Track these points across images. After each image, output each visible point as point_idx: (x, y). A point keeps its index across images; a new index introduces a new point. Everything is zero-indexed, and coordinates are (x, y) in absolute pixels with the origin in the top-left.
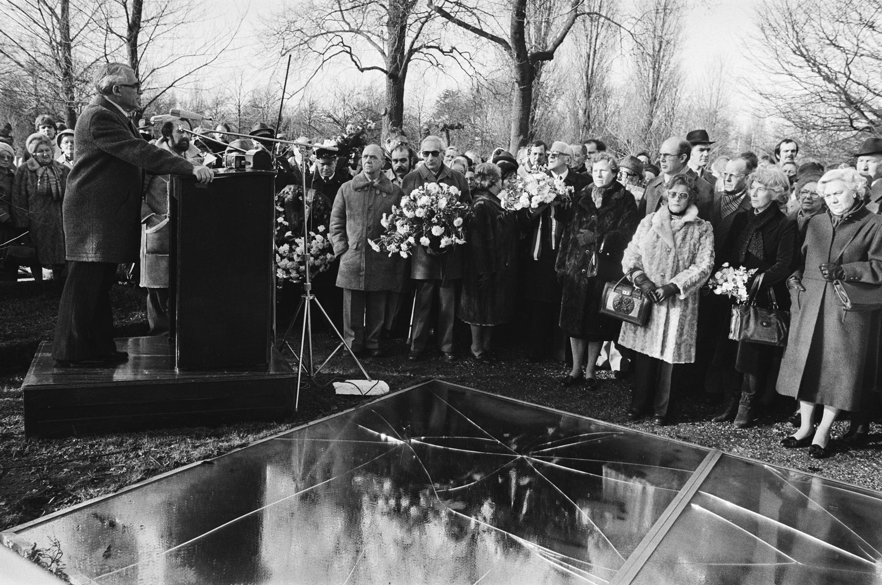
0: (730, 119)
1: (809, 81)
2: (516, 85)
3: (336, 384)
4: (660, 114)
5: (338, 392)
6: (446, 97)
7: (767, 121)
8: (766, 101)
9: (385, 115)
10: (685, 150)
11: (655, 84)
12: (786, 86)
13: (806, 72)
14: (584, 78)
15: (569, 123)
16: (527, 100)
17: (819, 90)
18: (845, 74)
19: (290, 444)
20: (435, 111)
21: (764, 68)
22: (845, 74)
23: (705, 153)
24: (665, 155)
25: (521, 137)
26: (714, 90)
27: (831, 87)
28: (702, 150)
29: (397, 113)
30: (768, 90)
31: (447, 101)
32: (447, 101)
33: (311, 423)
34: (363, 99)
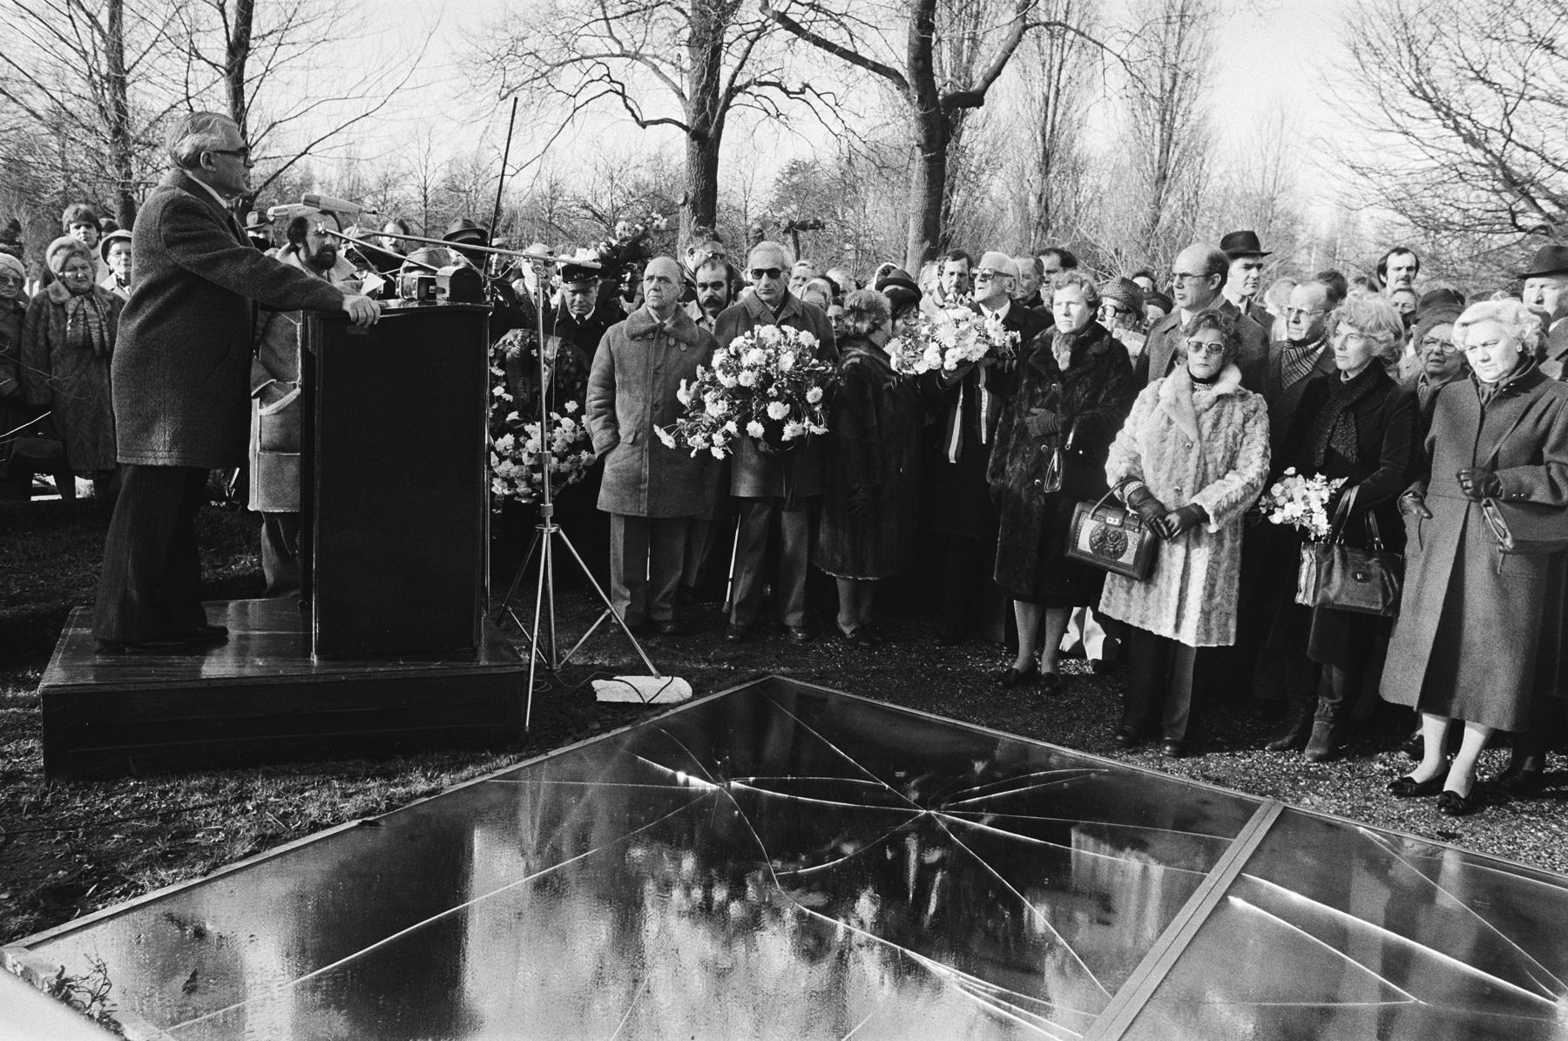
0: (1297, 212)
1: (1438, 143)
2: (918, 151)
3: (596, 684)
4: (1173, 202)
5: (601, 697)
6: (792, 172)
7: (1364, 215)
8: (1362, 180)
9: (684, 204)
10: (1217, 268)
11: (1165, 150)
12: (1398, 154)
13: (1432, 127)
14: (1039, 138)
15: (1011, 220)
16: (938, 179)
17: (1457, 159)
18: (1502, 131)
19: (516, 790)
20: (774, 198)
21: (1358, 121)
22: (1502, 131)
23: (1254, 272)
24: (1183, 276)
25: (927, 244)
26: (1270, 160)
27: (1478, 155)
28: (1248, 267)
29: (705, 201)
30: (1366, 159)
31: (795, 179)
32: (795, 179)
33: (553, 753)
34: (646, 176)
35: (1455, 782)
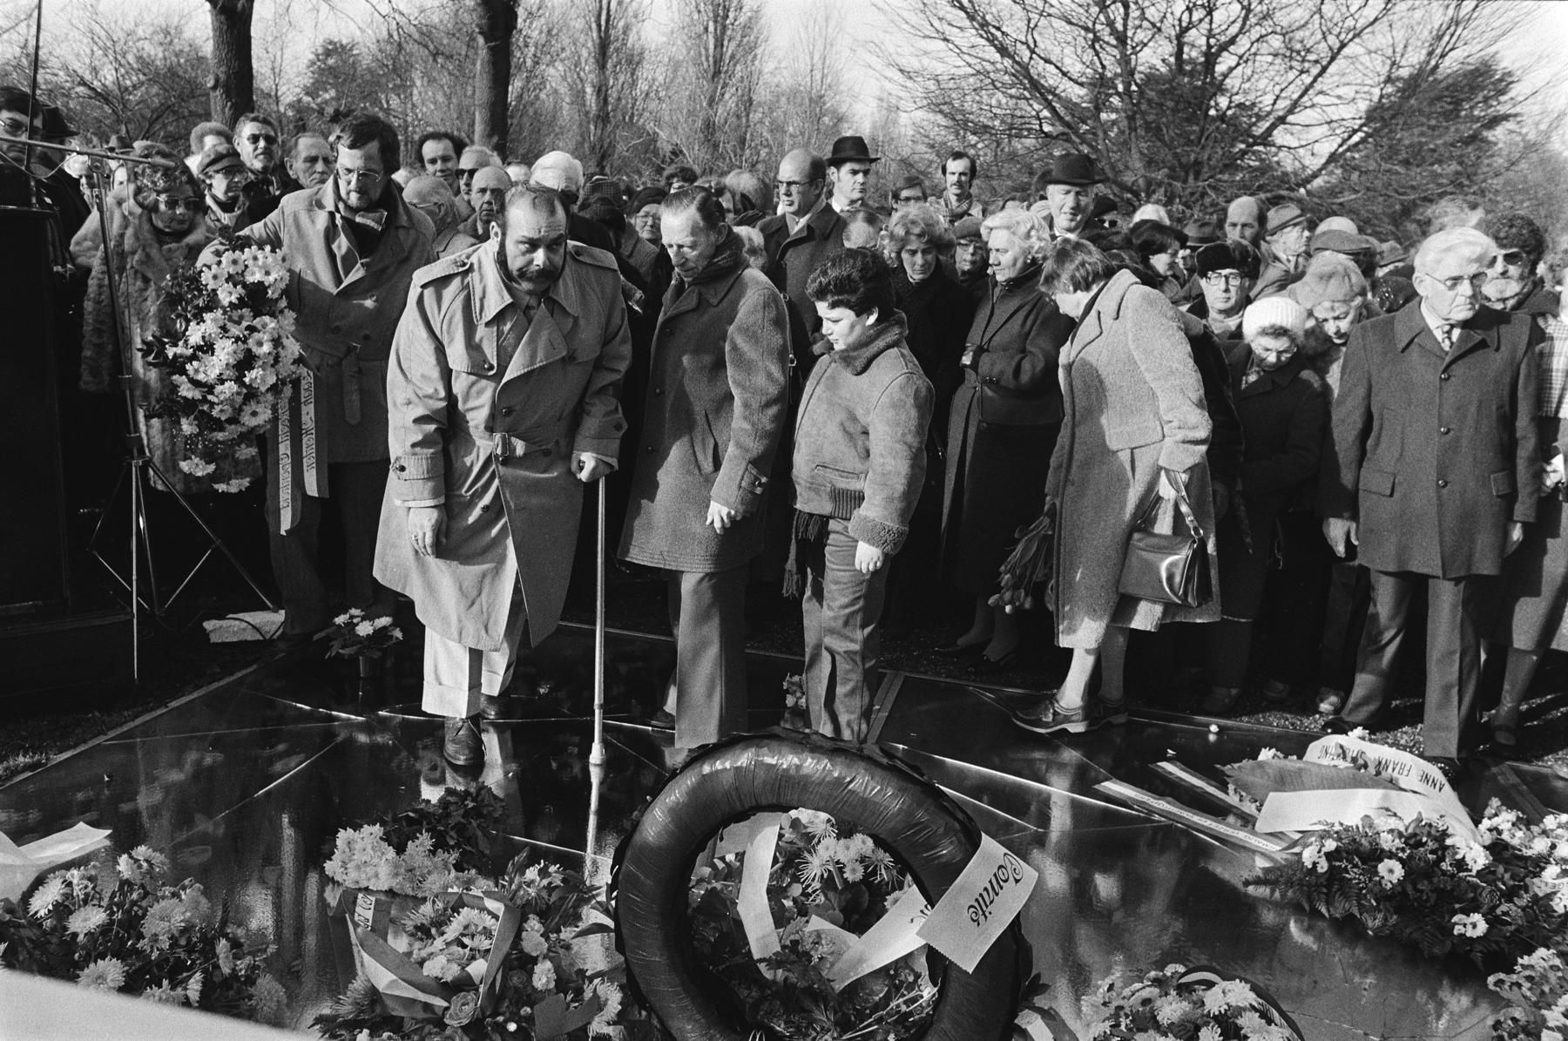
0: (843, 109)
1: (972, 52)
2: (481, 40)
3: (209, 625)
4: (730, 101)
5: (214, 639)
6: (328, 53)
7: (903, 118)
8: (909, 84)
9: (214, 88)
10: (816, 175)
11: (719, 43)
12: (941, 60)
13: (969, 37)
14: (594, 26)
15: (567, 112)
16: (501, 67)
17: (989, 67)
18: (1026, 43)
19: (130, 748)
20: (308, 81)
21: (905, 26)
22: (1026, 43)
23: (860, 178)
24: (789, 184)
25: (495, 139)
26: (816, 57)
27: (1008, 62)
28: (855, 172)
29: (239, 86)
30: (912, 64)
31: (331, 61)
32: (331, 61)
33: (174, 704)
34: (154, 51)
35: (993, 652)
